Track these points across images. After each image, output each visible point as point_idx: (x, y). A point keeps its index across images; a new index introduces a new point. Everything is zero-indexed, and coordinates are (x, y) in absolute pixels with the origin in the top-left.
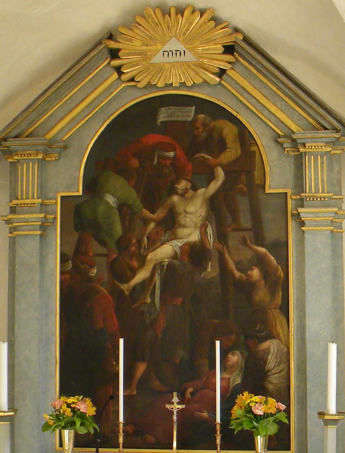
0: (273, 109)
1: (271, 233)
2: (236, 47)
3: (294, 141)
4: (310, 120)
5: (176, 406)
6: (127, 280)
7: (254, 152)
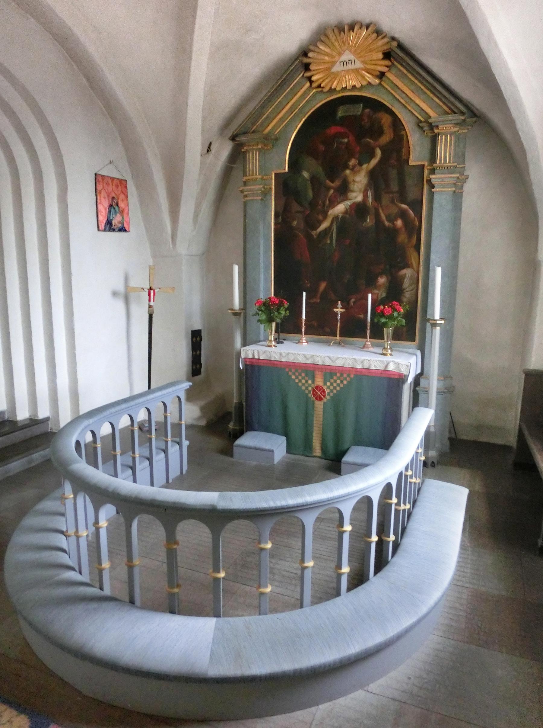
0: (418, 101)
1: (412, 195)
2: (392, 53)
3: (431, 124)
4: (445, 107)
5: (339, 310)
6: (315, 229)
7: (403, 135)
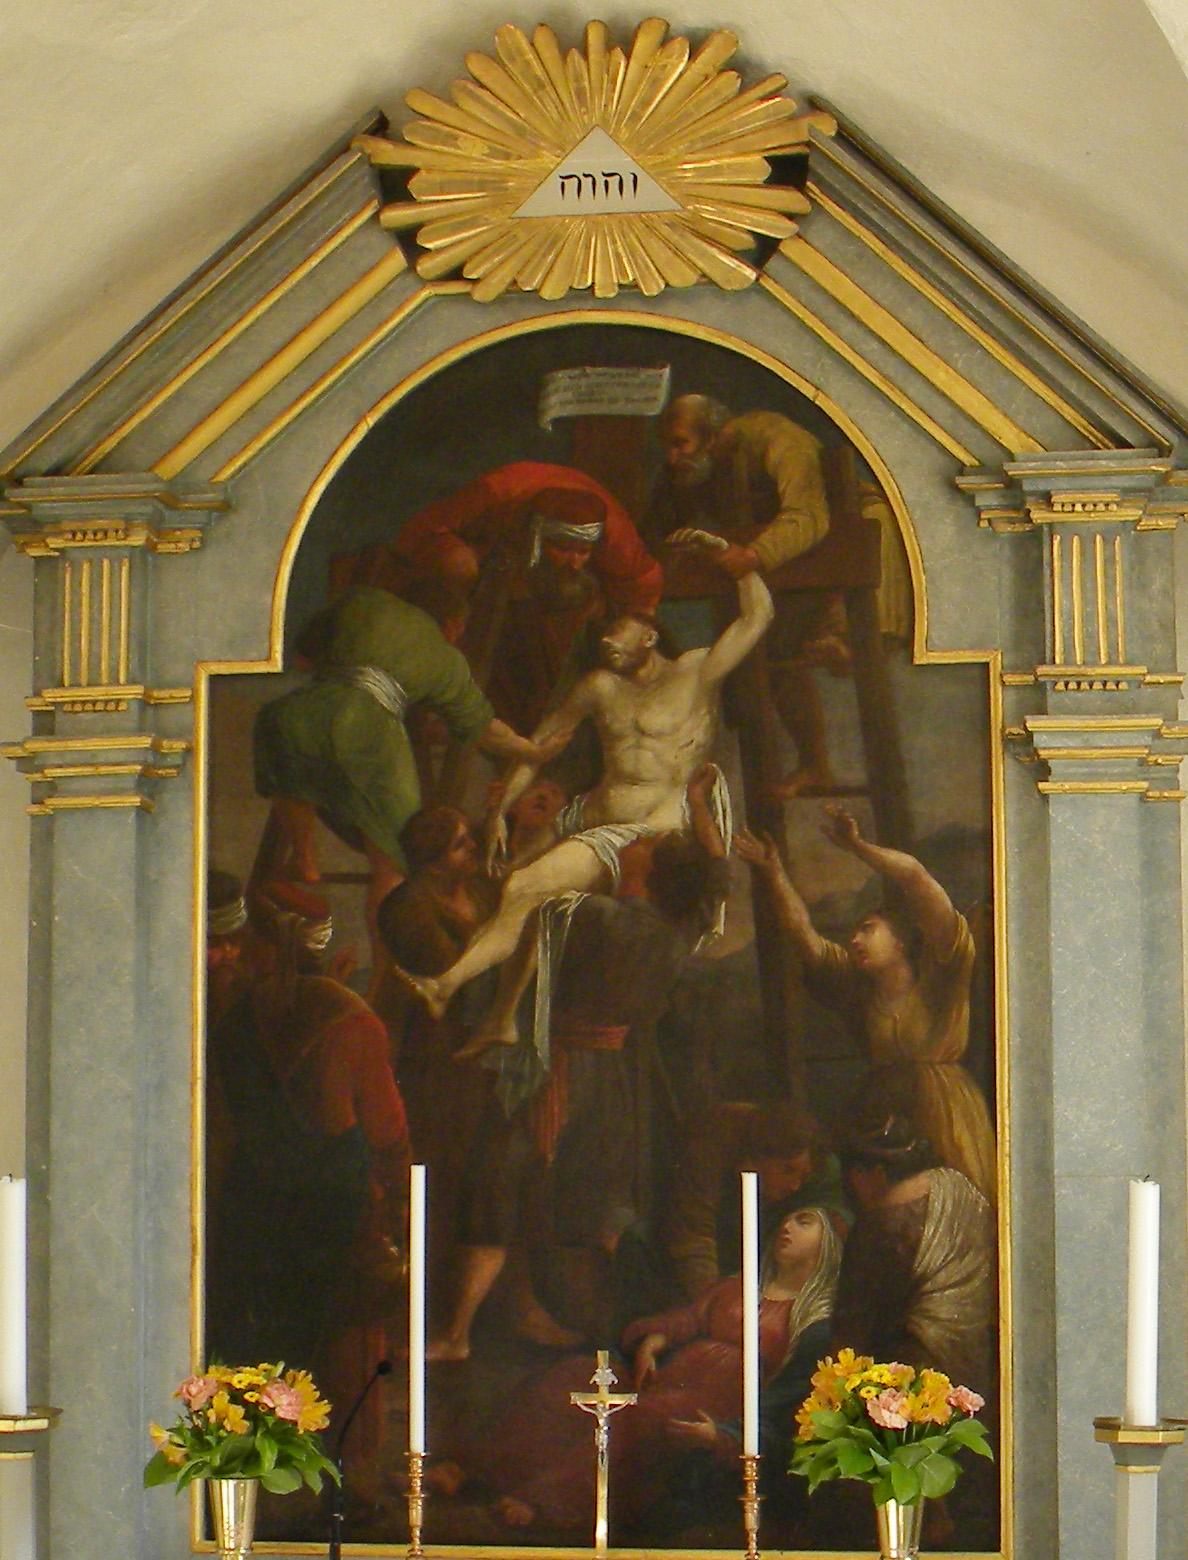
0: (941, 376)
1: (934, 803)
2: (811, 162)
3: (1012, 484)
4: (1069, 413)
5: (605, 1398)
6: (438, 966)
7: (875, 524)
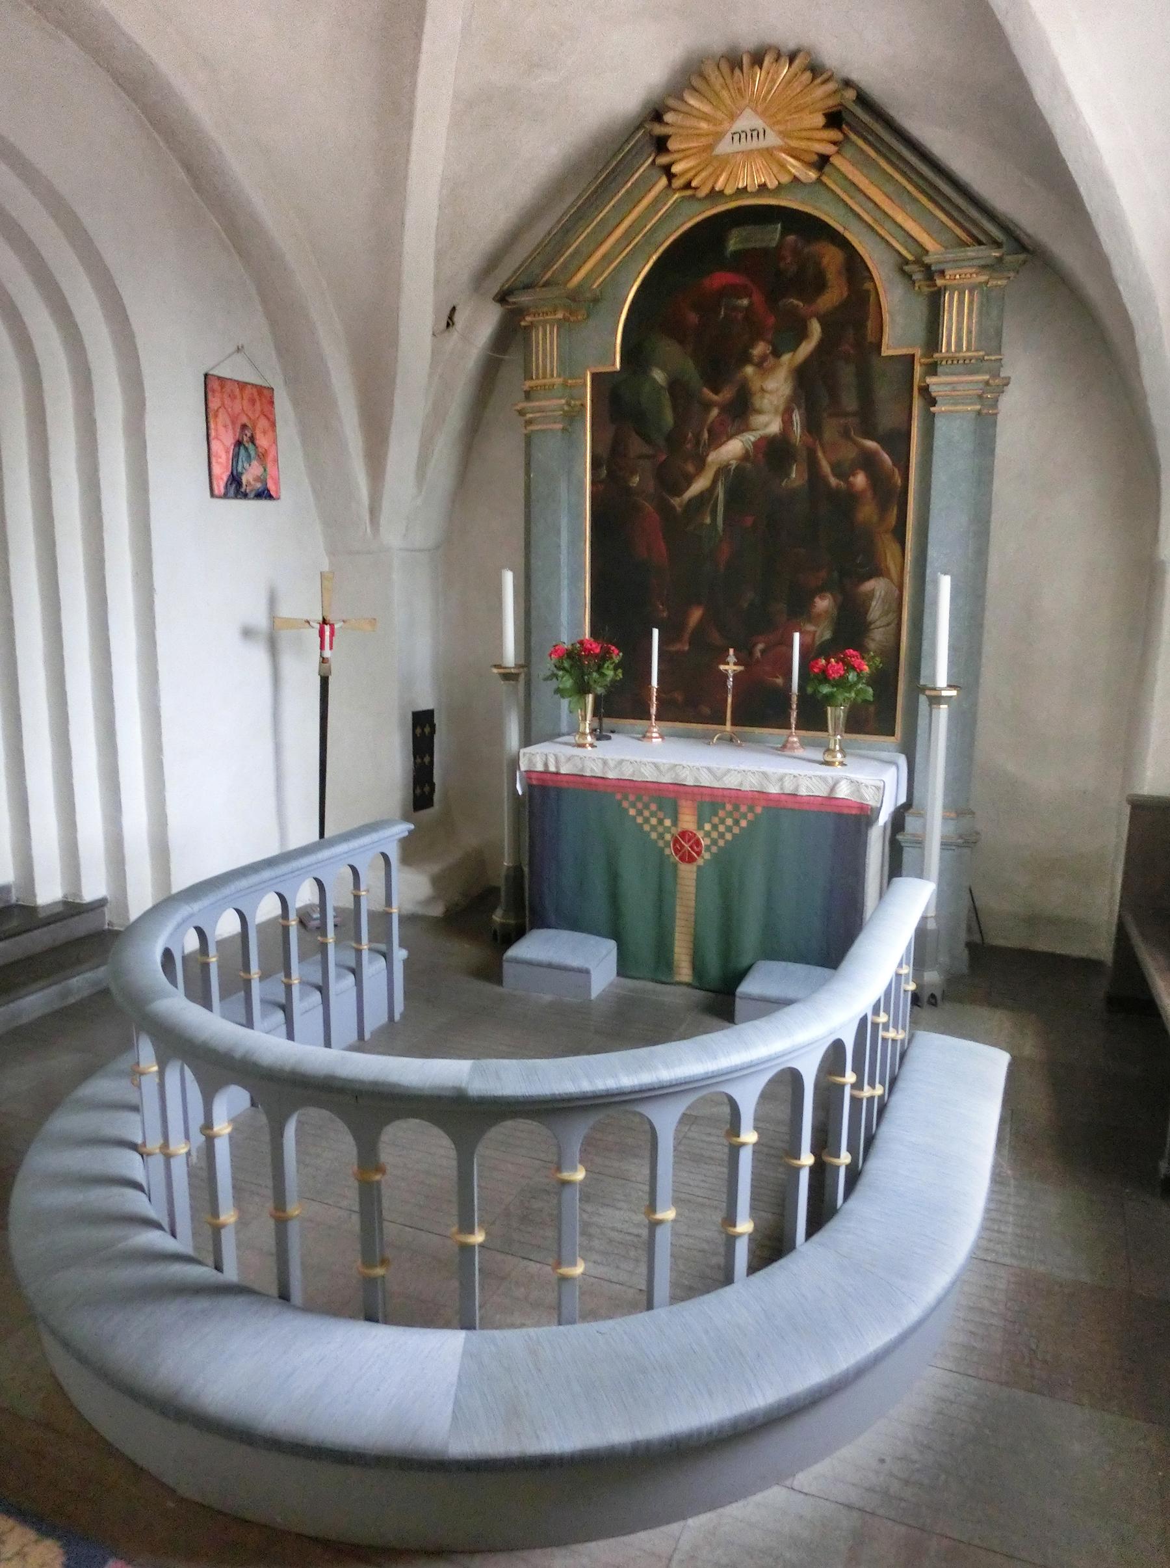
0: (900, 218)
1: (887, 419)
2: (844, 114)
3: (928, 267)
4: (958, 231)
5: (730, 668)
6: (680, 493)
7: (868, 291)
